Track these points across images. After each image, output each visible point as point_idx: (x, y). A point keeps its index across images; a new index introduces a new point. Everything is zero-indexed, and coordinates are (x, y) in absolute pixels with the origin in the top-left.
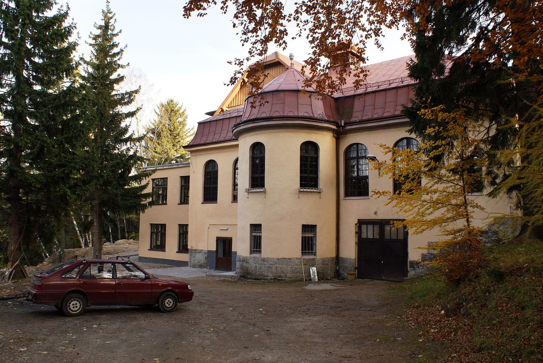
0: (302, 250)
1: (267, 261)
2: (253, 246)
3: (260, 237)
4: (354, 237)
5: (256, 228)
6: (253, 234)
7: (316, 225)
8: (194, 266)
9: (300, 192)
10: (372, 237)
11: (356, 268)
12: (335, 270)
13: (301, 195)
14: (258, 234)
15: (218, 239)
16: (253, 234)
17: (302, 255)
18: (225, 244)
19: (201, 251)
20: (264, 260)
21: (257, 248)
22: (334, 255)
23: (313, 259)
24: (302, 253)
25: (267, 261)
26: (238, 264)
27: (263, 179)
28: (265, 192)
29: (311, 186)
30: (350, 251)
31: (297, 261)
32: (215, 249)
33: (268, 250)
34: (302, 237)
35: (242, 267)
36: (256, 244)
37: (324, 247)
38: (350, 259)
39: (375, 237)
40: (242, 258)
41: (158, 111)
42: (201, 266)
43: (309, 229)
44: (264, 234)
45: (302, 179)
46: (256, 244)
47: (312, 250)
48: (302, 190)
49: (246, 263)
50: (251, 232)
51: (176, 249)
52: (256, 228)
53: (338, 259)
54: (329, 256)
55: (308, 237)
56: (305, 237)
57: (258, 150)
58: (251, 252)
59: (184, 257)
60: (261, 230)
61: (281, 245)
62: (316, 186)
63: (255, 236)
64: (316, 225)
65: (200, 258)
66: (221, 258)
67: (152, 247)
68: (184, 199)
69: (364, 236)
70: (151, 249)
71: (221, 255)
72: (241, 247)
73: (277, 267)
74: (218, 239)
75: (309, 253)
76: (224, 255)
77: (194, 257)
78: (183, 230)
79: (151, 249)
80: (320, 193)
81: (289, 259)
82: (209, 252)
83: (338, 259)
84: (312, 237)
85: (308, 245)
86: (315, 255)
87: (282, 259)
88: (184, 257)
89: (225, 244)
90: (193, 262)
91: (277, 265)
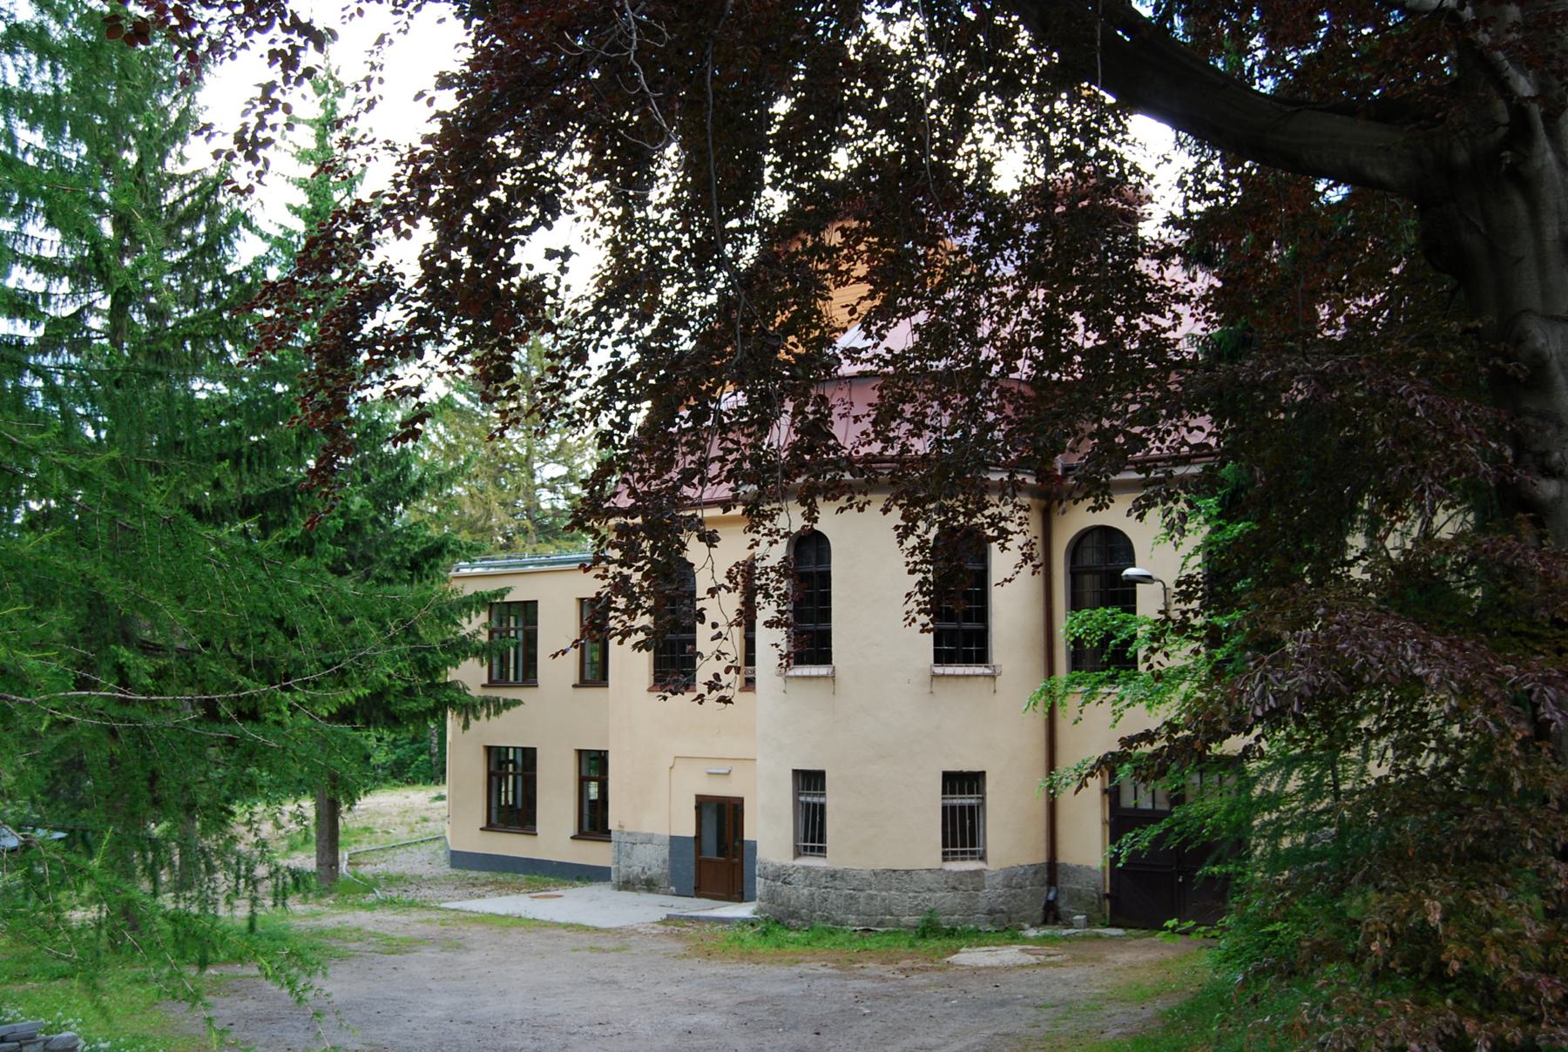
0: (945, 845)
1: (842, 878)
2: (802, 835)
3: (823, 806)
4: (1099, 808)
5: (810, 781)
6: (802, 799)
7: (984, 773)
8: (627, 885)
9: (934, 676)
10: (1150, 806)
11: (1107, 896)
12: (1047, 898)
13: (938, 687)
14: (816, 800)
15: (702, 803)
16: (802, 799)
17: (945, 860)
18: (721, 817)
19: (649, 839)
20: (833, 875)
21: (813, 841)
22: (1041, 858)
23: (978, 873)
24: (944, 854)
25: (842, 878)
26: (760, 886)
27: (825, 638)
28: (832, 677)
29: (967, 659)
30: (1088, 846)
31: (928, 876)
32: (692, 833)
33: (846, 848)
34: (944, 808)
35: (772, 896)
36: (812, 828)
37: (1009, 840)
38: (1088, 868)
39: (1158, 807)
40: (771, 869)
41: (678, 947)
42: (650, 885)
43: (962, 782)
44: (834, 800)
45: (936, 652)
46: (812, 828)
47: (973, 844)
48: (939, 670)
49: (784, 882)
50: (797, 793)
51: (572, 828)
52: (810, 781)
53: (1052, 870)
54: (1027, 860)
55: (962, 808)
56: (953, 808)
57: (810, 552)
58: (798, 852)
59: (593, 854)
60: (823, 788)
61: (884, 831)
62: (982, 657)
63: (808, 804)
64: (984, 773)
65: (652, 859)
66: (709, 861)
67: (494, 820)
68: (595, 674)
69: (1127, 801)
70: (490, 826)
71: (710, 850)
72: (769, 832)
73: (872, 897)
74: (702, 803)
75: (963, 853)
76: (720, 852)
77: (628, 856)
78: (594, 765)
79: (490, 826)
80: (993, 677)
81: (907, 872)
82: (674, 840)
83: (1052, 870)
84: (971, 808)
85: (962, 828)
86: (983, 858)
87: (885, 871)
88: (593, 854)
89: (721, 817)
90: (623, 871)
91: (873, 892)
